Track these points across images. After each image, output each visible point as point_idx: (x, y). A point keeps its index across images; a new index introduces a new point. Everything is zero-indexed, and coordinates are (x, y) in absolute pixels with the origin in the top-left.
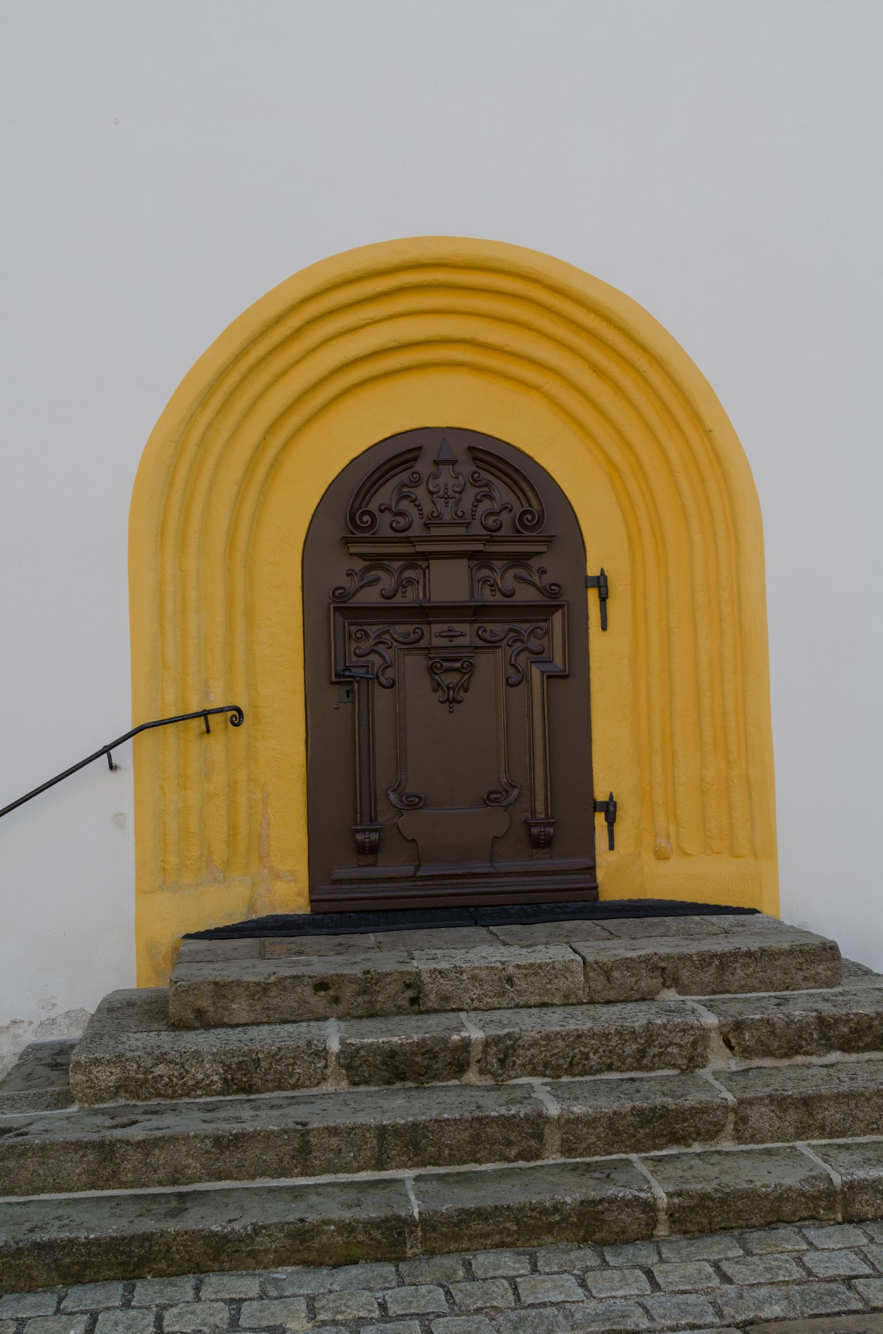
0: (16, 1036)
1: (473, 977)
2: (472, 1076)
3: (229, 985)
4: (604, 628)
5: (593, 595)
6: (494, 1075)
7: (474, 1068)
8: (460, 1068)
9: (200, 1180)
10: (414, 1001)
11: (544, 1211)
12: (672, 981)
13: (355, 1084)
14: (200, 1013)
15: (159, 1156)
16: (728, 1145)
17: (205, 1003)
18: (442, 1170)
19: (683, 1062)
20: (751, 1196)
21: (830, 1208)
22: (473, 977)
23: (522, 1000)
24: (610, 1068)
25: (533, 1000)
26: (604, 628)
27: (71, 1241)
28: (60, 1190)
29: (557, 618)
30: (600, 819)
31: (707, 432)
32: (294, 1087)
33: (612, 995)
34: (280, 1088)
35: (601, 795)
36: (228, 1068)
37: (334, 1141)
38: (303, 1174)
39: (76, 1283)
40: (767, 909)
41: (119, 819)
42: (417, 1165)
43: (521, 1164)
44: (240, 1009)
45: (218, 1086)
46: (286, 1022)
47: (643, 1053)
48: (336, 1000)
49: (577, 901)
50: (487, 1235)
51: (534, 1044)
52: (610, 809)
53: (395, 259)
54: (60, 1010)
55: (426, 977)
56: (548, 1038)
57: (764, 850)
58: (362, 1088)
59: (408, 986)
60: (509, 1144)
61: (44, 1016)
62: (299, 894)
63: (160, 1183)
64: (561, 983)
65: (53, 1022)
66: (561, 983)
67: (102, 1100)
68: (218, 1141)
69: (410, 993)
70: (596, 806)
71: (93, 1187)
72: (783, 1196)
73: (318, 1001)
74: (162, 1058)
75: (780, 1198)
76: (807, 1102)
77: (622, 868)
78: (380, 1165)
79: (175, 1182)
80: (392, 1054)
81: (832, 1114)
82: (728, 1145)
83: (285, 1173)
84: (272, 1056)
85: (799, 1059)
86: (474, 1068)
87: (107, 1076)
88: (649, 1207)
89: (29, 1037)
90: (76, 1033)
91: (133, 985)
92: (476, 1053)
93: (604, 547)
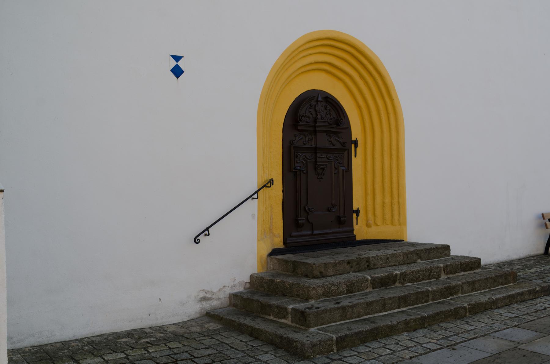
0: (225, 291)
1: (381, 258)
2: (397, 284)
3: (327, 264)
4: (355, 156)
5: (353, 146)
6: (402, 283)
7: (398, 282)
8: (394, 282)
9: (363, 316)
10: (368, 266)
11: (449, 312)
12: (420, 257)
13: (373, 288)
14: (321, 273)
15: (355, 309)
16: (460, 295)
17: (322, 270)
18: (411, 307)
19: (437, 277)
20: (481, 303)
21: (494, 306)
22: (381, 258)
23: (390, 264)
24: (423, 280)
25: (393, 264)
26: (355, 156)
27: (363, 331)
28: (334, 322)
29: (346, 152)
30: (355, 215)
31: (392, 99)
32: (362, 290)
33: (408, 261)
34: (358, 291)
35: (355, 208)
36: (347, 286)
37: (390, 301)
38: (385, 311)
39: (374, 340)
40: (405, 240)
41: (253, 215)
42: (407, 306)
43: (425, 304)
44: (330, 271)
45: (345, 292)
46: (341, 274)
47: (429, 275)
48: (352, 267)
49: (351, 242)
50: (439, 319)
51: (410, 274)
52: (357, 212)
53: (324, 36)
54: (236, 282)
55: (371, 259)
56: (412, 272)
57: (402, 223)
58: (375, 290)
59: (367, 262)
60: (423, 299)
61: (232, 284)
62: (281, 241)
63: (356, 318)
64: (398, 259)
65: (235, 286)
66: (398, 259)
67: (319, 298)
68: (367, 303)
69: (367, 264)
70: (354, 211)
71: (341, 320)
72: (486, 303)
73: (347, 267)
74: (333, 284)
75: (486, 304)
76: (473, 283)
77: (361, 230)
78: (399, 308)
79: (359, 317)
80: (382, 279)
81: (477, 285)
82: (460, 295)
83: (381, 312)
84: (357, 282)
85: (457, 274)
86: (398, 282)
87: (321, 291)
88: (465, 308)
89: (228, 291)
90: (242, 289)
91: (256, 272)
92: (398, 277)
93: (356, 133)
